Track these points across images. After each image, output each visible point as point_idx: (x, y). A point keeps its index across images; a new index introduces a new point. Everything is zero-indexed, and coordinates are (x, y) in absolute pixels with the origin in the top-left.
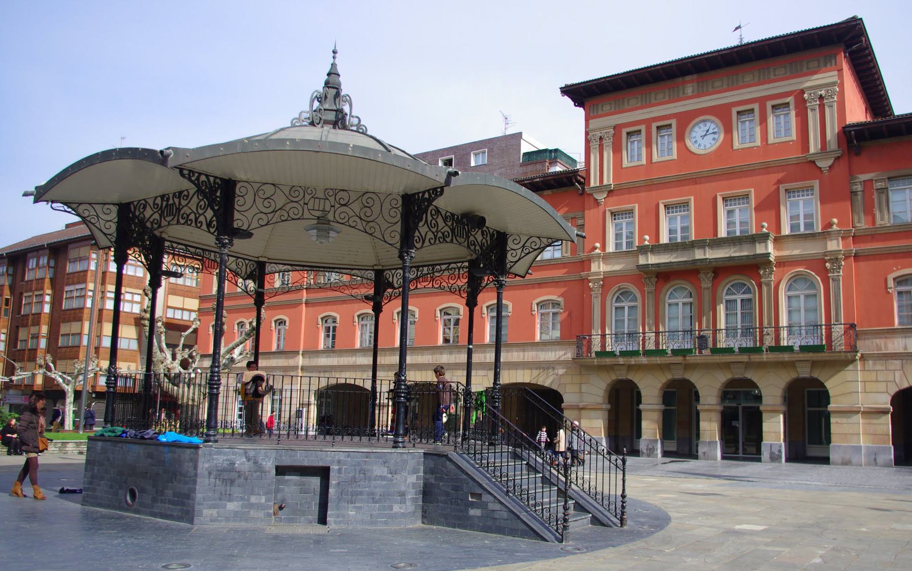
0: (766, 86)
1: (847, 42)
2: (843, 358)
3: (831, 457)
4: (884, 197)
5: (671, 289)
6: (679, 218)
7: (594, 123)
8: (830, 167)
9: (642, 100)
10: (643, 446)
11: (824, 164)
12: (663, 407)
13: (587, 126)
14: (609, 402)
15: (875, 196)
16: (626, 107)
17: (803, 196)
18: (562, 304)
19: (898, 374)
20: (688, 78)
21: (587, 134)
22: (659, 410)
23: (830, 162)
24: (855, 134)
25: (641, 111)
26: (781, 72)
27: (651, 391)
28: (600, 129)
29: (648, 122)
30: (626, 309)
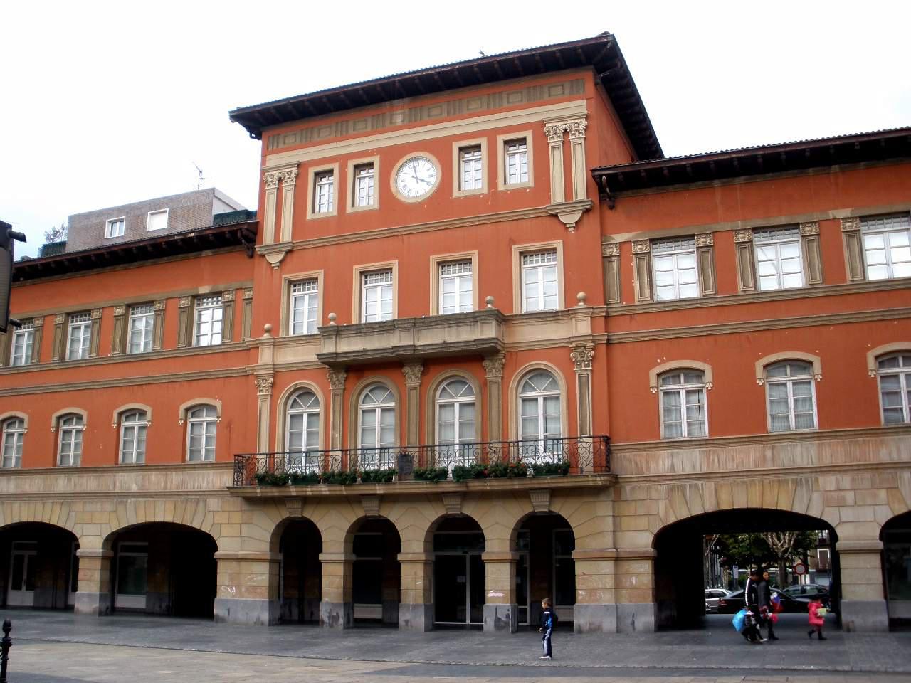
0: (497, 116)
2: (591, 483)
3: (575, 622)
4: (855, 241)
5: (446, 383)
6: (307, 297)
7: (273, 160)
8: (576, 223)
9: (336, 132)
10: (324, 613)
12: (354, 557)
13: (263, 162)
15: (634, 264)
16: (316, 139)
17: (309, 289)
18: (219, 408)
19: (662, 505)
20: (397, 102)
21: (263, 173)
23: (577, 217)
24: (607, 181)
25: (333, 145)
26: (515, 98)
29: (491, 134)
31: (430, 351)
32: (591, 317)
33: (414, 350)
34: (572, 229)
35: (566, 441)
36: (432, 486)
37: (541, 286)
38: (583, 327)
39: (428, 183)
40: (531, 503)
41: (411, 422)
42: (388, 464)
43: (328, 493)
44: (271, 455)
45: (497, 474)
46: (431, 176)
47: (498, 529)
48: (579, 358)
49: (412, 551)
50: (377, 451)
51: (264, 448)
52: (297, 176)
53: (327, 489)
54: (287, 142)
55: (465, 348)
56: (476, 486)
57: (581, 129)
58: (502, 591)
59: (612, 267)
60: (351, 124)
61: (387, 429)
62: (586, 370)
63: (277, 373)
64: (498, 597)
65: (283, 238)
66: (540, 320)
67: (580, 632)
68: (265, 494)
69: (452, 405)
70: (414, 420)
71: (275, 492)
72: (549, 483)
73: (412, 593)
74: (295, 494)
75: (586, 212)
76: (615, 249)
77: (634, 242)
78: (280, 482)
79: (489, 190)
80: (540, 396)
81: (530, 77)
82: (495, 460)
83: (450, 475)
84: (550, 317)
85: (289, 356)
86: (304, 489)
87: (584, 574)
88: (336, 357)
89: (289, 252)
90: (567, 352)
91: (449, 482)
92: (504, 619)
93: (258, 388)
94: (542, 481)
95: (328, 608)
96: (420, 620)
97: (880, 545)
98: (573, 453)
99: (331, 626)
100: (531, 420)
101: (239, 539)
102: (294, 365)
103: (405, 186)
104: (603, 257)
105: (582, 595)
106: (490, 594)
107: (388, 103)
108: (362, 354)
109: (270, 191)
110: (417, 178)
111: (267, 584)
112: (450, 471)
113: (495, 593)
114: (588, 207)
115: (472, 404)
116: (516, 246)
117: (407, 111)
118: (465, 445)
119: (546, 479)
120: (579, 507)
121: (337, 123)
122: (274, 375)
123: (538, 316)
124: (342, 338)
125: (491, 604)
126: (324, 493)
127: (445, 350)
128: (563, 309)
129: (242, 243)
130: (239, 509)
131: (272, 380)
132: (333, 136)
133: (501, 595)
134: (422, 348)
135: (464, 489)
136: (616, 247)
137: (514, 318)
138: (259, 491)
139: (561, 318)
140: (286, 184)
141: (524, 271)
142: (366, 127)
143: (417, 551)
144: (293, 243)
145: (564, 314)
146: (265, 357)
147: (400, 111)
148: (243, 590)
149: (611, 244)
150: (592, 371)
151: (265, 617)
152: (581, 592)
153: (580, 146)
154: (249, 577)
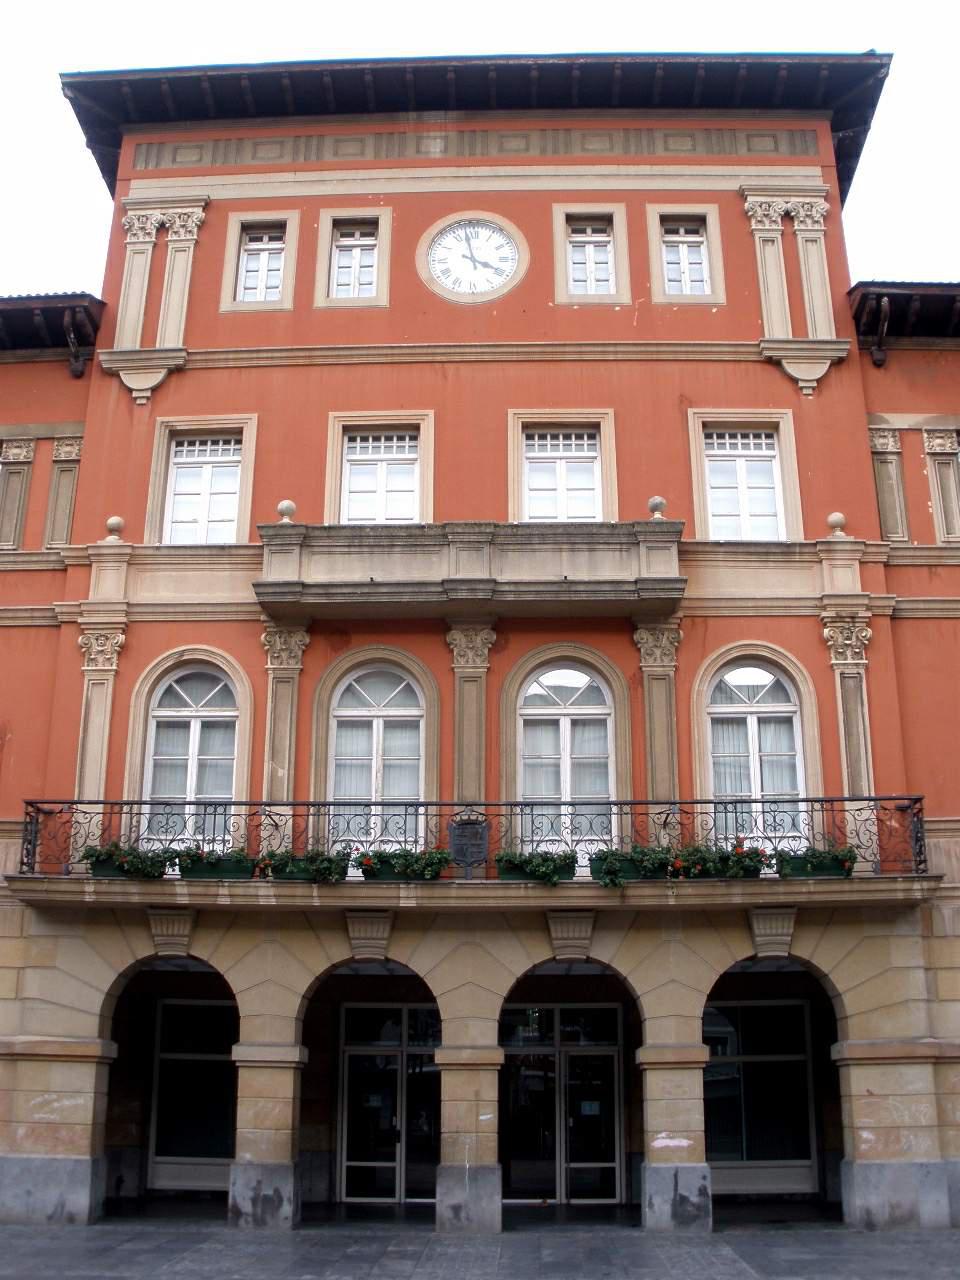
1: (828, 101)
2: (900, 896)
8: (154, 390)
9: (296, 153)
11: (808, 372)
14: (115, 1037)
16: (248, 160)
20: (432, 117)
22: (100, 1061)
23: (820, 370)
26: (681, 145)
27: (269, 994)
28: (163, 203)
30: (195, 727)
31: (530, 597)
32: (861, 563)
33: (494, 591)
34: (810, 391)
35: (433, 810)
36: (538, 893)
37: (746, 495)
38: (844, 579)
39: (498, 271)
40: (550, 939)
41: (465, 753)
42: (413, 837)
43: (273, 902)
44: (113, 805)
45: (670, 873)
46: (503, 259)
47: (673, 994)
48: (840, 640)
49: (468, 1043)
50: (146, 809)
51: (93, 786)
52: (201, 226)
53: (272, 892)
54: (178, 159)
55: (611, 597)
56: (644, 895)
57: (192, 224)
58: (685, 1132)
59: (888, 472)
60: (329, 142)
61: (166, 766)
62: (857, 664)
63: (135, 627)
64: (678, 1148)
65: (163, 340)
66: (754, 558)
67: (870, 1225)
68: (240, 901)
69: (184, 725)
70: (472, 746)
71: (133, 893)
72: (809, 893)
73: (468, 1140)
74: (184, 900)
75: (837, 363)
76: (891, 440)
77: (928, 431)
78: (147, 869)
79: (633, 301)
80: (751, 713)
81: (710, 111)
82: (665, 842)
83: (583, 872)
84: (774, 553)
85: (161, 589)
86: (213, 890)
87: (870, 1094)
88: (302, 594)
89: (175, 371)
90: (819, 623)
91: (582, 885)
92: (694, 1199)
93: (83, 653)
94: (796, 889)
95: (254, 1175)
96: (491, 1204)
97: (703, 1054)
98: (835, 829)
99: (259, 1222)
100: (400, 767)
101: (18, 1004)
102: (750, 604)
103: (446, 272)
104: (873, 453)
105: (867, 1141)
106: (659, 1142)
107: (413, 115)
108: (366, 590)
109: (139, 247)
110: (473, 259)
111: (88, 1117)
112: (583, 861)
113: (671, 1138)
114: (844, 354)
115: (411, 725)
116: (696, 410)
117: (453, 135)
118: (207, 804)
119: (804, 883)
120: (850, 953)
121: (138, 145)
122: (126, 629)
123: (752, 549)
124: (314, 553)
125: (662, 1165)
126: (262, 902)
127: (564, 597)
128: (800, 538)
129: (66, 345)
130: (18, 934)
131: (122, 638)
132: (287, 160)
133: (685, 1143)
134: (512, 588)
135: (614, 902)
136: (894, 436)
137: (700, 548)
138: (90, 888)
139: (797, 558)
140: (175, 238)
141: (172, 470)
142: (362, 154)
143: (481, 1042)
144: (189, 354)
145: (806, 550)
146: (108, 586)
147: (438, 134)
148: (21, 1131)
149: (884, 430)
150: (867, 667)
151: (81, 1200)
152: (865, 1135)
153: (143, 256)
154: (39, 1099)
